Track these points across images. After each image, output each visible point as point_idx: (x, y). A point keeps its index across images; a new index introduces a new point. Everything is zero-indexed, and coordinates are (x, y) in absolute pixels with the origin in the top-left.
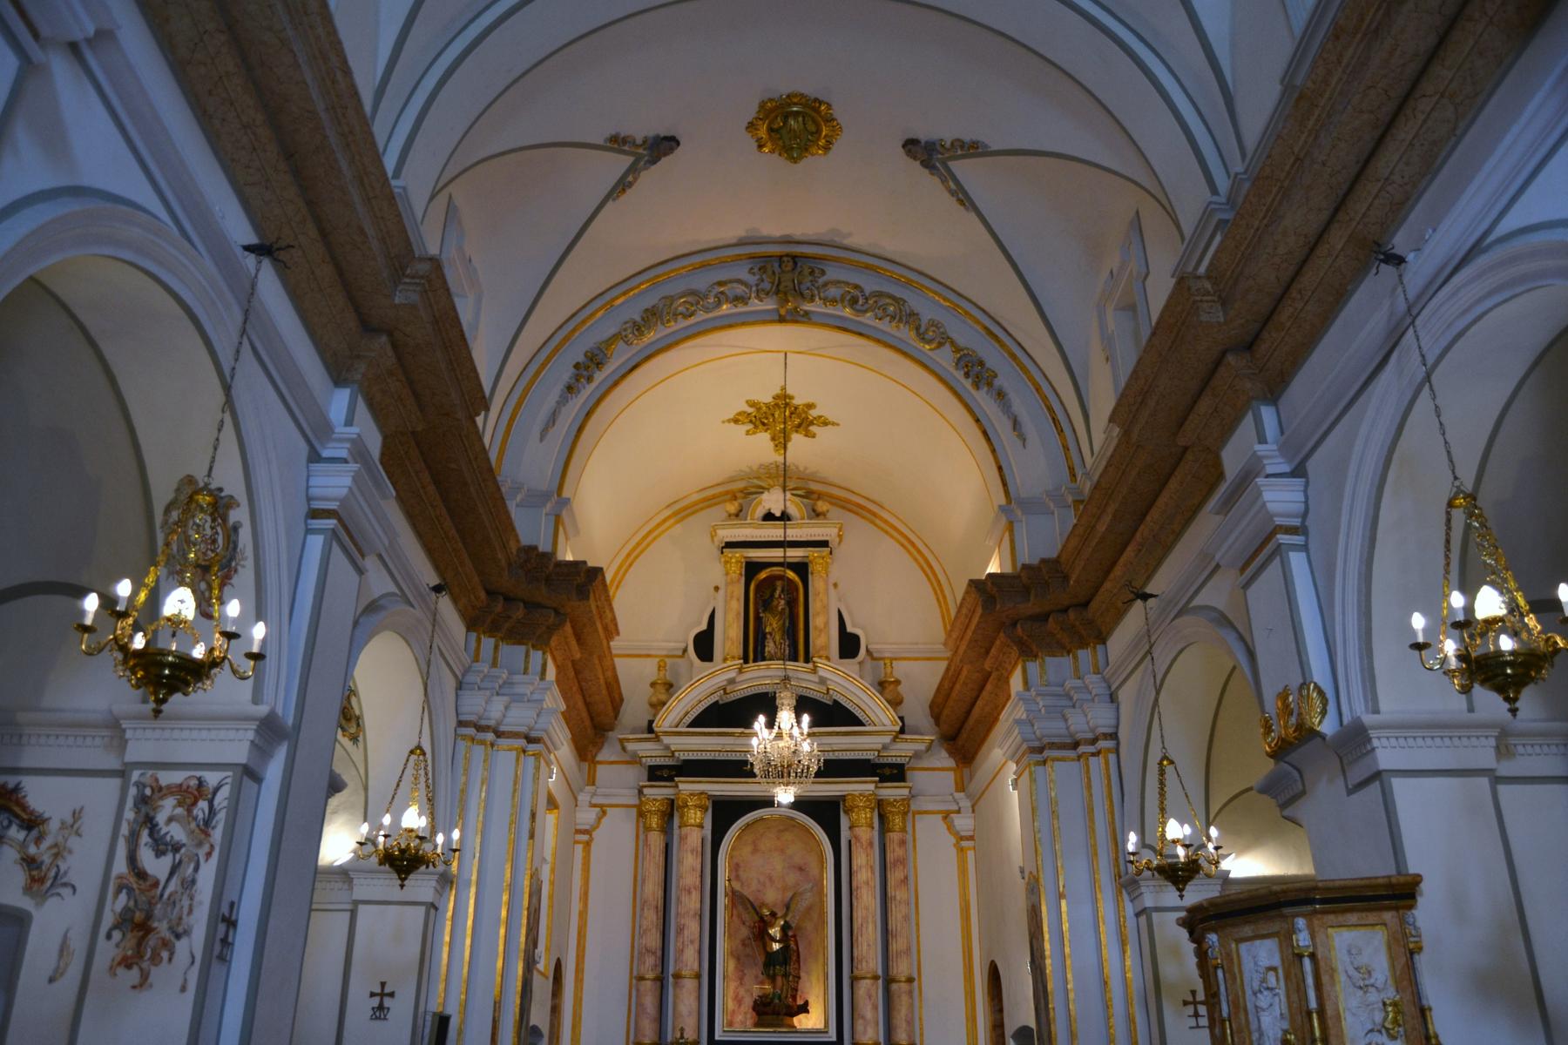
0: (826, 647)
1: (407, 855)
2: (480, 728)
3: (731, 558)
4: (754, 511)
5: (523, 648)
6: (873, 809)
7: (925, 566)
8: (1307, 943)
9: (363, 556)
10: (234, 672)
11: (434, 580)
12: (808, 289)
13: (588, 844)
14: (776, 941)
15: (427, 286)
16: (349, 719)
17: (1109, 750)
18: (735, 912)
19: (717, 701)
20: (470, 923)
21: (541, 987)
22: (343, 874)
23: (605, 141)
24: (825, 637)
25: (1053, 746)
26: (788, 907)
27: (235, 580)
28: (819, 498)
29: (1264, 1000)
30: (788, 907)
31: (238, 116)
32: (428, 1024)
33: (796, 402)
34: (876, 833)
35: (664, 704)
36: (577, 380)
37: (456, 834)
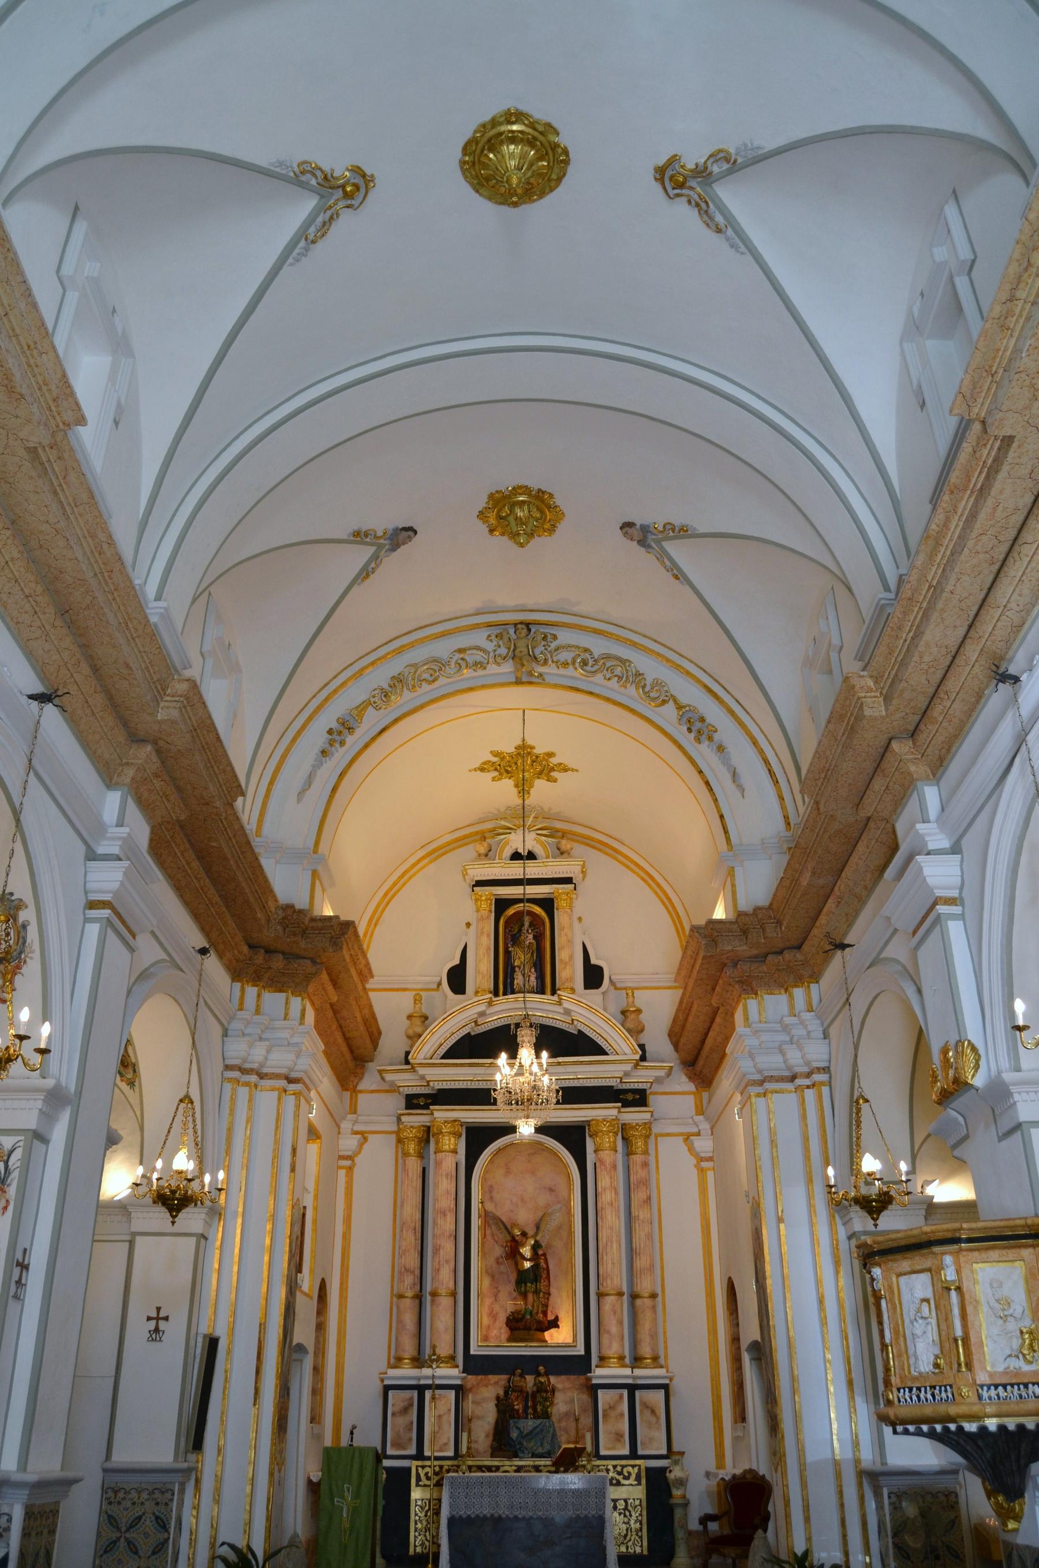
0: (571, 979)
1: (177, 1195)
2: (245, 1071)
3: (481, 896)
4: (502, 850)
5: (283, 995)
6: (616, 1134)
7: (665, 900)
8: (953, 1278)
9: (134, 937)
10: (25, 1064)
11: (202, 942)
12: (542, 653)
13: (350, 1169)
14: (527, 1260)
15: (185, 702)
16: (127, 1066)
17: (823, 1083)
18: (488, 1232)
19: (469, 1033)
20: (237, 1251)
21: (306, 1308)
22: (122, 1208)
23: (348, 536)
24: (569, 970)
25: (771, 1079)
26: (538, 1227)
27: (24, 970)
28: (563, 837)
29: (919, 1327)
30: (538, 1227)
31: (22, 590)
32: (200, 1345)
33: (536, 751)
34: (620, 1156)
35: (420, 1036)
36: (331, 745)
37: (221, 1175)
